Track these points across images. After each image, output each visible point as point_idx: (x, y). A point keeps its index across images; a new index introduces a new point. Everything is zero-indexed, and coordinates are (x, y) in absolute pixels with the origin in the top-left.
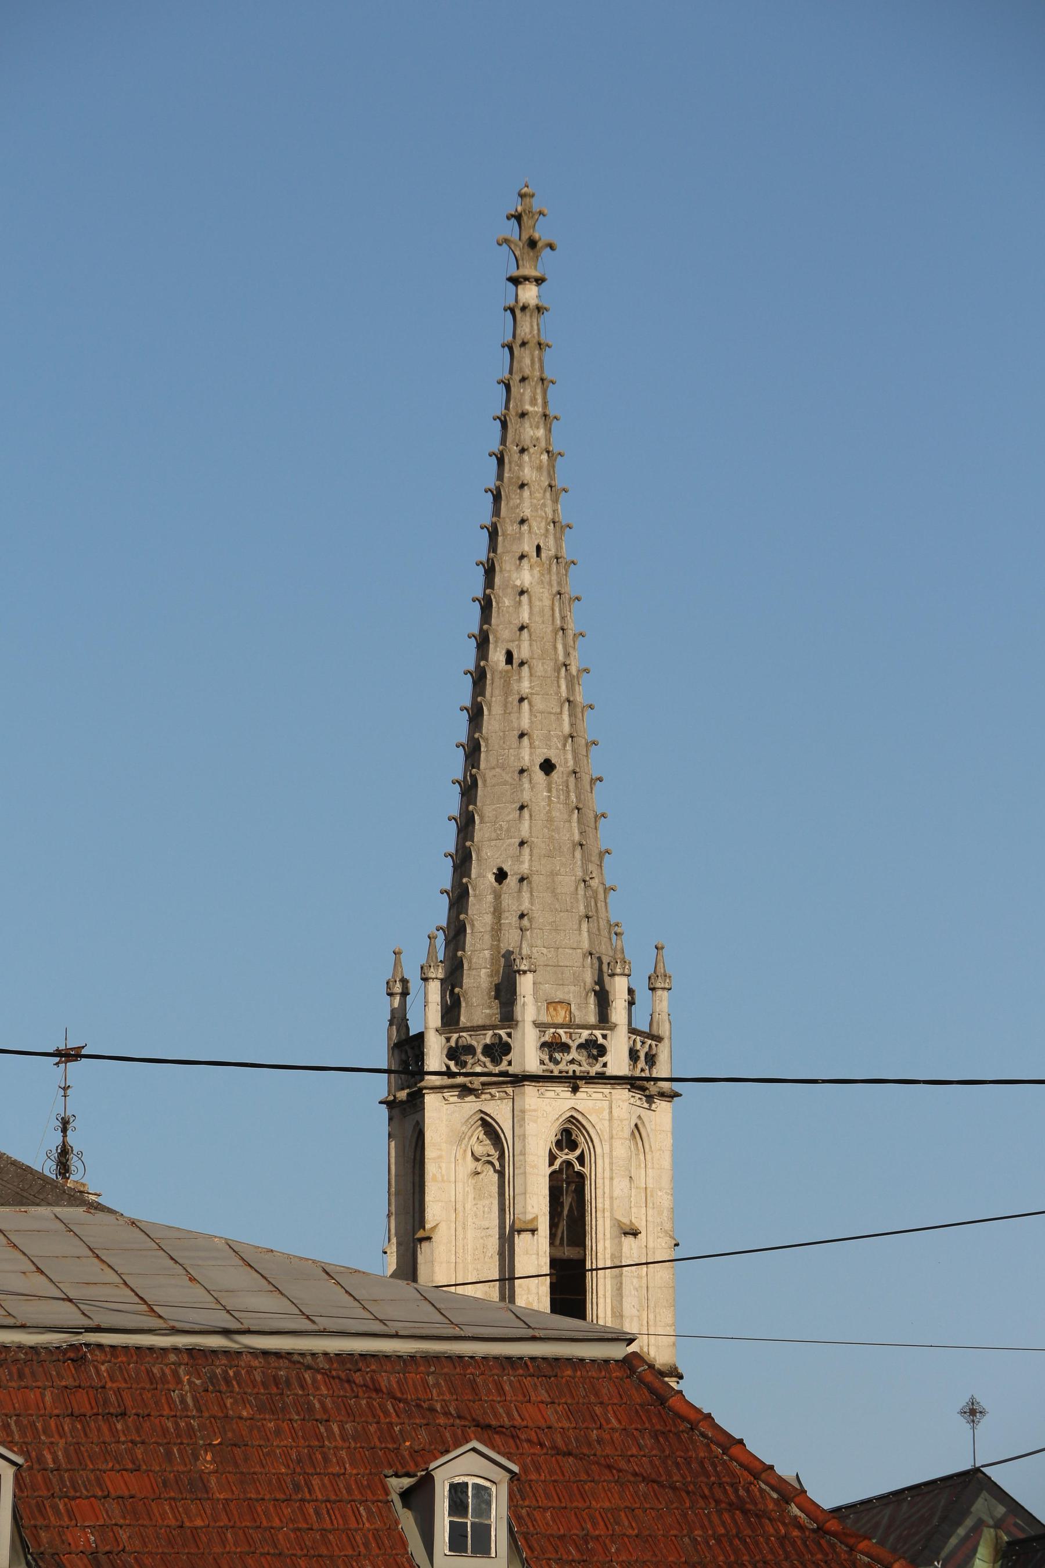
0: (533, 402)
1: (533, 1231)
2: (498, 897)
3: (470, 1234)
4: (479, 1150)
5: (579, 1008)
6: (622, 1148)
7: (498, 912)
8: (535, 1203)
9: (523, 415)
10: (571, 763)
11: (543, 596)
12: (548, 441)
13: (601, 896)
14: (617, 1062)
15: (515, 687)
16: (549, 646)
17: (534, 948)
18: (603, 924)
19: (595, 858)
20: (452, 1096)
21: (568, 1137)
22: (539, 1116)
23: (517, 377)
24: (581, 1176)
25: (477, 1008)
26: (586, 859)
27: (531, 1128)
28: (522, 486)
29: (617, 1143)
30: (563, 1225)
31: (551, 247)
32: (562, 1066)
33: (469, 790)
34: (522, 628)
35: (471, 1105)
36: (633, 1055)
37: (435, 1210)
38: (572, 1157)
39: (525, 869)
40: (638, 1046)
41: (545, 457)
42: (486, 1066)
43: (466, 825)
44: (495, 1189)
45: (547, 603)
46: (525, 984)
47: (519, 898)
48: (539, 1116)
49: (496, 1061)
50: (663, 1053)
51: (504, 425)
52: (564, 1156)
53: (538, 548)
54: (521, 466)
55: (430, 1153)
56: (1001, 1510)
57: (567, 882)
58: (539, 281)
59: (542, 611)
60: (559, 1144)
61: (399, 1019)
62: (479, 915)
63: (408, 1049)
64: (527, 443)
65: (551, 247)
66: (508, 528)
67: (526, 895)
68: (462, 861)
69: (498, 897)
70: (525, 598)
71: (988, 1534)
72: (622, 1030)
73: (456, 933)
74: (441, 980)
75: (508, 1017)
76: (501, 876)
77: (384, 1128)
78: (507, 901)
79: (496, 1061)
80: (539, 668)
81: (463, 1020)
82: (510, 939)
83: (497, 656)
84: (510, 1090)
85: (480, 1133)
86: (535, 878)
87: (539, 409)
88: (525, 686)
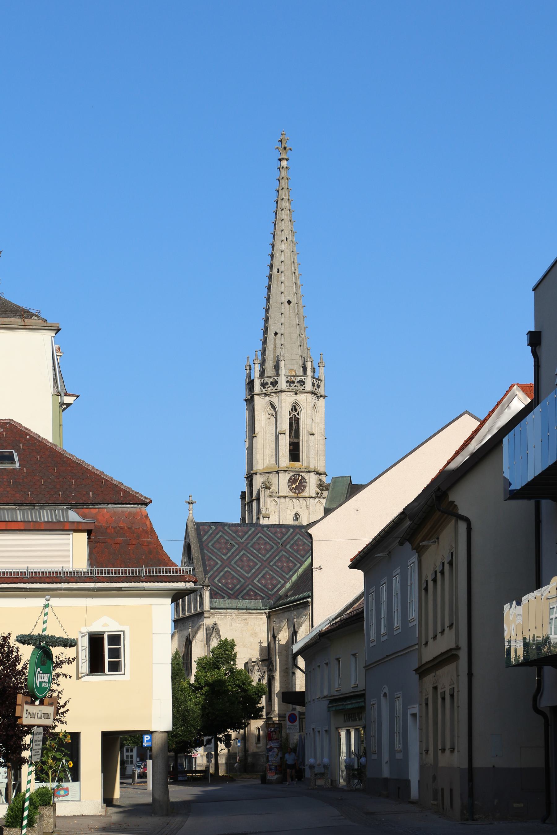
0: (285, 195)
1: (284, 434)
2: (275, 340)
3: (267, 435)
4: (270, 412)
5: (298, 371)
7: (275, 345)
8: (285, 426)
9: (282, 199)
10: (296, 301)
11: (288, 252)
12: (289, 207)
13: (305, 340)
14: (308, 386)
15: (280, 279)
16: (290, 267)
17: (283, 353)
18: (305, 348)
19: (303, 329)
20: (262, 396)
21: (294, 408)
22: (286, 402)
23: (281, 188)
24: (298, 419)
26: (300, 329)
27: (283, 405)
28: (282, 220)
30: (293, 432)
31: (290, 149)
32: (292, 388)
33: (267, 310)
34: (282, 262)
35: (267, 399)
36: (313, 385)
37: (257, 429)
38: (296, 413)
39: (282, 331)
40: (315, 382)
41: (289, 211)
42: (271, 385)
43: (266, 320)
45: (289, 254)
46: (282, 364)
49: (274, 386)
50: (322, 384)
51: (277, 203)
52: (293, 413)
53: (287, 238)
54: (282, 214)
55: (256, 413)
57: (295, 335)
58: (287, 160)
60: (292, 410)
61: (249, 376)
63: (251, 384)
64: (283, 207)
65: (290, 149)
66: (278, 233)
67: (283, 339)
68: (266, 330)
69: (275, 340)
70: (283, 253)
73: (264, 351)
75: (278, 374)
76: (276, 334)
77: (245, 407)
78: (277, 341)
79: (274, 386)
80: (287, 273)
81: (265, 375)
82: (278, 352)
83: (275, 270)
84: (278, 394)
85: (270, 407)
86: (285, 334)
87: (287, 197)
88: (283, 279)
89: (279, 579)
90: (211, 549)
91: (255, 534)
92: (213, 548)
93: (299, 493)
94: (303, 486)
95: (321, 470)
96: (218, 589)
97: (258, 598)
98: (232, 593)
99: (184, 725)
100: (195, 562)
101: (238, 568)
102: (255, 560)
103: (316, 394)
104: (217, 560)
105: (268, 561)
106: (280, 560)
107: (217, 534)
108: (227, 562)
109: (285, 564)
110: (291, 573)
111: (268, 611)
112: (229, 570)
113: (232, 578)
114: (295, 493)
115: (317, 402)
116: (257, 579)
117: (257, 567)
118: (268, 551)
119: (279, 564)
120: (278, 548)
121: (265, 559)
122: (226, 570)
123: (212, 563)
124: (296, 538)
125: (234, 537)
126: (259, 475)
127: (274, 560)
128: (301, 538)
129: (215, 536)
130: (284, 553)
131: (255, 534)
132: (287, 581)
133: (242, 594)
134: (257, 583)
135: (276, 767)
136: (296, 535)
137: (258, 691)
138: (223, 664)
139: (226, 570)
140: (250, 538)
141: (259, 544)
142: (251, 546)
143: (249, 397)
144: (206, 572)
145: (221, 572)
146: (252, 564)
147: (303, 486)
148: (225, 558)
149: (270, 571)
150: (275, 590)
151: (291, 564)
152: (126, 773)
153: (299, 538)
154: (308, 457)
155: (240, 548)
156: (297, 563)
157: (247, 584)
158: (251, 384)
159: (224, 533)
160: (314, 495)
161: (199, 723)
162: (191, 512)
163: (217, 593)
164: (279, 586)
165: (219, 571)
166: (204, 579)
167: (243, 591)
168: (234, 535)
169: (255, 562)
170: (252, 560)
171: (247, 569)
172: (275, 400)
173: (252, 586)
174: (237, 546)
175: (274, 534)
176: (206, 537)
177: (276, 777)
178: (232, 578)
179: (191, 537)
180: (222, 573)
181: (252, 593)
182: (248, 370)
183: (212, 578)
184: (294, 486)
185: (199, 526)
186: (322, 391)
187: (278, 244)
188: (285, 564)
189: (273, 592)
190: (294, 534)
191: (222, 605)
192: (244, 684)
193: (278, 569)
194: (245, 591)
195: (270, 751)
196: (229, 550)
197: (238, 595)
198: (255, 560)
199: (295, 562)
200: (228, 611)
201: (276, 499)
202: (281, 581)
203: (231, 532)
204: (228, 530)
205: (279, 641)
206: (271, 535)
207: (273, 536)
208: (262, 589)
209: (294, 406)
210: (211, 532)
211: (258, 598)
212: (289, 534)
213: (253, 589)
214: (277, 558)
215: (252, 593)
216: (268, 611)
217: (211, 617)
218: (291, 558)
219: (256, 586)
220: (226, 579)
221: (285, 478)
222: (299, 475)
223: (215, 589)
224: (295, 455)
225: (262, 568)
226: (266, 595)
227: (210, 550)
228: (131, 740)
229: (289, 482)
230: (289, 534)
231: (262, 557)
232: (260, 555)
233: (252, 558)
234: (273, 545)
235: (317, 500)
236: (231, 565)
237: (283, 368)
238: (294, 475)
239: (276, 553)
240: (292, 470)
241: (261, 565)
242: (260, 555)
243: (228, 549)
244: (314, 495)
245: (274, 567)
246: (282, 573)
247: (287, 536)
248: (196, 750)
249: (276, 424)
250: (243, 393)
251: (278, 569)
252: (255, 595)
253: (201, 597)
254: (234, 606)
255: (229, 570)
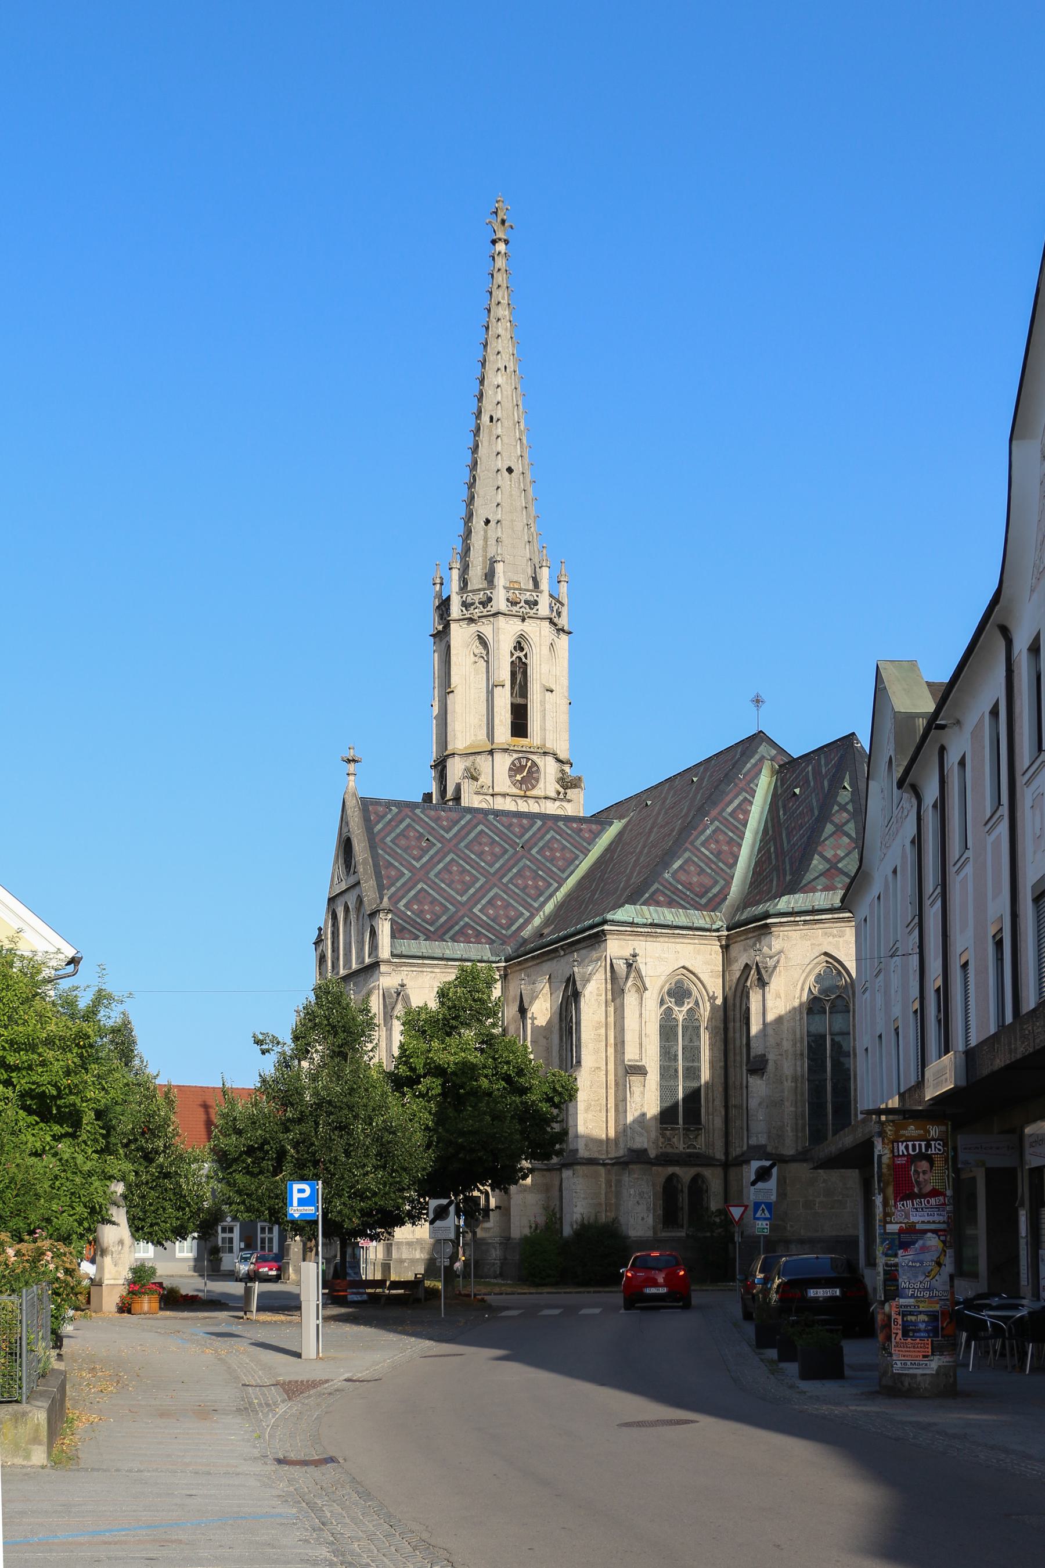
2: (486, 532)
4: (477, 652)
6: (545, 650)
7: (486, 539)
8: (504, 674)
9: (499, 303)
11: (508, 389)
17: (503, 551)
20: (464, 624)
21: (519, 646)
22: (504, 633)
23: (495, 287)
24: (525, 664)
25: (476, 579)
26: (528, 516)
27: (502, 637)
29: (543, 648)
30: (517, 687)
31: (511, 227)
35: (473, 628)
37: (455, 680)
38: (521, 654)
39: (499, 517)
42: (480, 608)
44: (484, 670)
46: (499, 568)
47: (496, 532)
48: (504, 633)
50: (565, 611)
52: (517, 654)
54: (497, 328)
56: (774, 752)
58: (506, 242)
59: (507, 397)
60: (515, 648)
62: (477, 541)
66: (491, 357)
67: (499, 530)
69: (486, 532)
71: (767, 764)
72: (546, 594)
73: (467, 550)
74: (445, 799)
78: (490, 533)
80: (506, 423)
83: (485, 418)
86: (503, 522)
87: (506, 302)
88: (499, 431)
89: (521, 908)
90: (390, 848)
91: (471, 826)
92: (393, 846)
93: (528, 789)
94: (534, 778)
95: (562, 756)
96: (405, 921)
97: (483, 940)
98: (432, 929)
99: (384, 1167)
100: (360, 869)
101: (443, 885)
102: (474, 872)
103: (555, 625)
104: (402, 869)
105: (498, 876)
106: (519, 874)
107: (401, 822)
108: (422, 872)
109: (530, 883)
110: (542, 899)
111: (504, 964)
112: (425, 887)
113: (431, 903)
114: (521, 789)
115: (556, 639)
116: (479, 906)
117: (478, 885)
118: (497, 858)
119: (520, 882)
120: (516, 852)
121: (492, 870)
122: (419, 886)
123: (393, 873)
124: (548, 836)
125: (433, 829)
126: (457, 758)
127: (510, 875)
128: (558, 837)
129: (397, 826)
130: (528, 863)
131: (471, 826)
132: (534, 912)
133: (452, 932)
134: (479, 913)
135: (933, 1316)
136: (547, 832)
137: (555, 1090)
138: (468, 1026)
139: (419, 886)
140: (463, 833)
141: (480, 844)
142: (466, 847)
143: (440, 628)
144: (381, 888)
145: (410, 890)
146: (468, 878)
147: (534, 778)
148: (418, 865)
149: (502, 894)
150: (514, 928)
151: (540, 883)
152: (222, 1268)
153: (553, 837)
154: (543, 729)
155: (446, 850)
156: (552, 881)
157: (460, 914)
158: (444, 606)
159: (413, 820)
160: (553, 795)
161: (425, 1162)
162: (352, 778)
163: (404, 928)
164: (521, 921)
165: (408, 886)
166: (378, 901)
167: (452, 927)
168: (433, 825)
169: (475, 876)
170: (468, 871)
171: (459, 887)
172: (486, 629)
173: (471, 919)
174: (439, 845)
175: (509, 827)
176: (380, 826)
177: (934, 1364)
178: (431, 903)
179: (351, 824)
180: (413, 893)
181: (470, 932)
182: (438, 586)
183: (395, 899)
184: (519, 777)
185: (366, 805)
186: (563, 622)
187: (490, 376)
188: (530, 883)
189: (510, 932)
190: (544, 830)
191: (414, 951)
192: (520, 1073)
193: (517, 891)
194: (457, 928)
195: (905, 1246)
196: (425, 851)
197: (445, 934)
198: (474, 872)
199: (549, 879)
200: (426, 962)
201: (489, 798)
202: (525, 911)
203: (427, 820)
204: (422, 816)
205: (533, 1019)
206: (502, 828)
207: (506, 831)
208: (488, 924)
209: (519, 643)
210: (389, 816)
211: (483, 940)
212: (535, 828)
213: (472, 923)
214: (515, 871)
215: (470, 932)
216: (504, 964)
217: (394, 973)
218: (540, 873)
219: (477, 920)
220: (420, 903)
221: (503, 762)
222: (528, 759)
223: (400, 921)
224: (520, 726)
225: (488, 886)
226: (497, 937)
227: (388, 850)
228: (243, 1202)
229: (510, 769)
230: (535, 828)
231: (487, 867)
232: (483, 864)
233: (468, 867)
234: (507, 846)
235: (558, 803)
236: (429, 879)
237: (501, 575)
238: (519, 759)
239: (512, 862)
240: (516, 748)
241: (485, 883)
242: (483, 864)
243: (422, 850)
244: (553, 795)
245: (510, 885)
246: (526, 897)
247: (531, 833)
248: (389, 1233)
249: (488, 672)
250: (431, 623)
251: (517, 891)
252: (477, 936)
253: (373, 933)
254: (438, 953)
255: (425, 887)
